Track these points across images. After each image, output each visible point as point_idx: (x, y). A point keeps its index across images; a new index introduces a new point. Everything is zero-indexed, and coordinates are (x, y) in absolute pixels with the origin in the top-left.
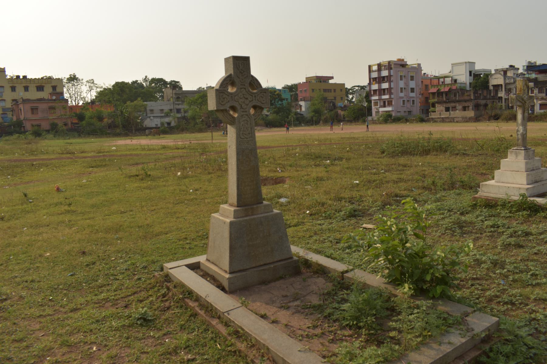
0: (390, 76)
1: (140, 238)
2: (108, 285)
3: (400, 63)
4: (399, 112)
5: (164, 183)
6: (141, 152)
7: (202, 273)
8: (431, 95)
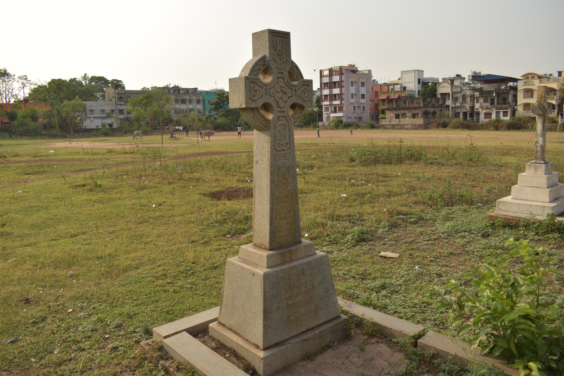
0: (341, 81)
1: (103, 275)
2: (70, 360)
3: (351, 69)
4: (350, 118)
5: (119, 195)
6: (84, 156)
7: (213, 344)
8: (381, 102)
